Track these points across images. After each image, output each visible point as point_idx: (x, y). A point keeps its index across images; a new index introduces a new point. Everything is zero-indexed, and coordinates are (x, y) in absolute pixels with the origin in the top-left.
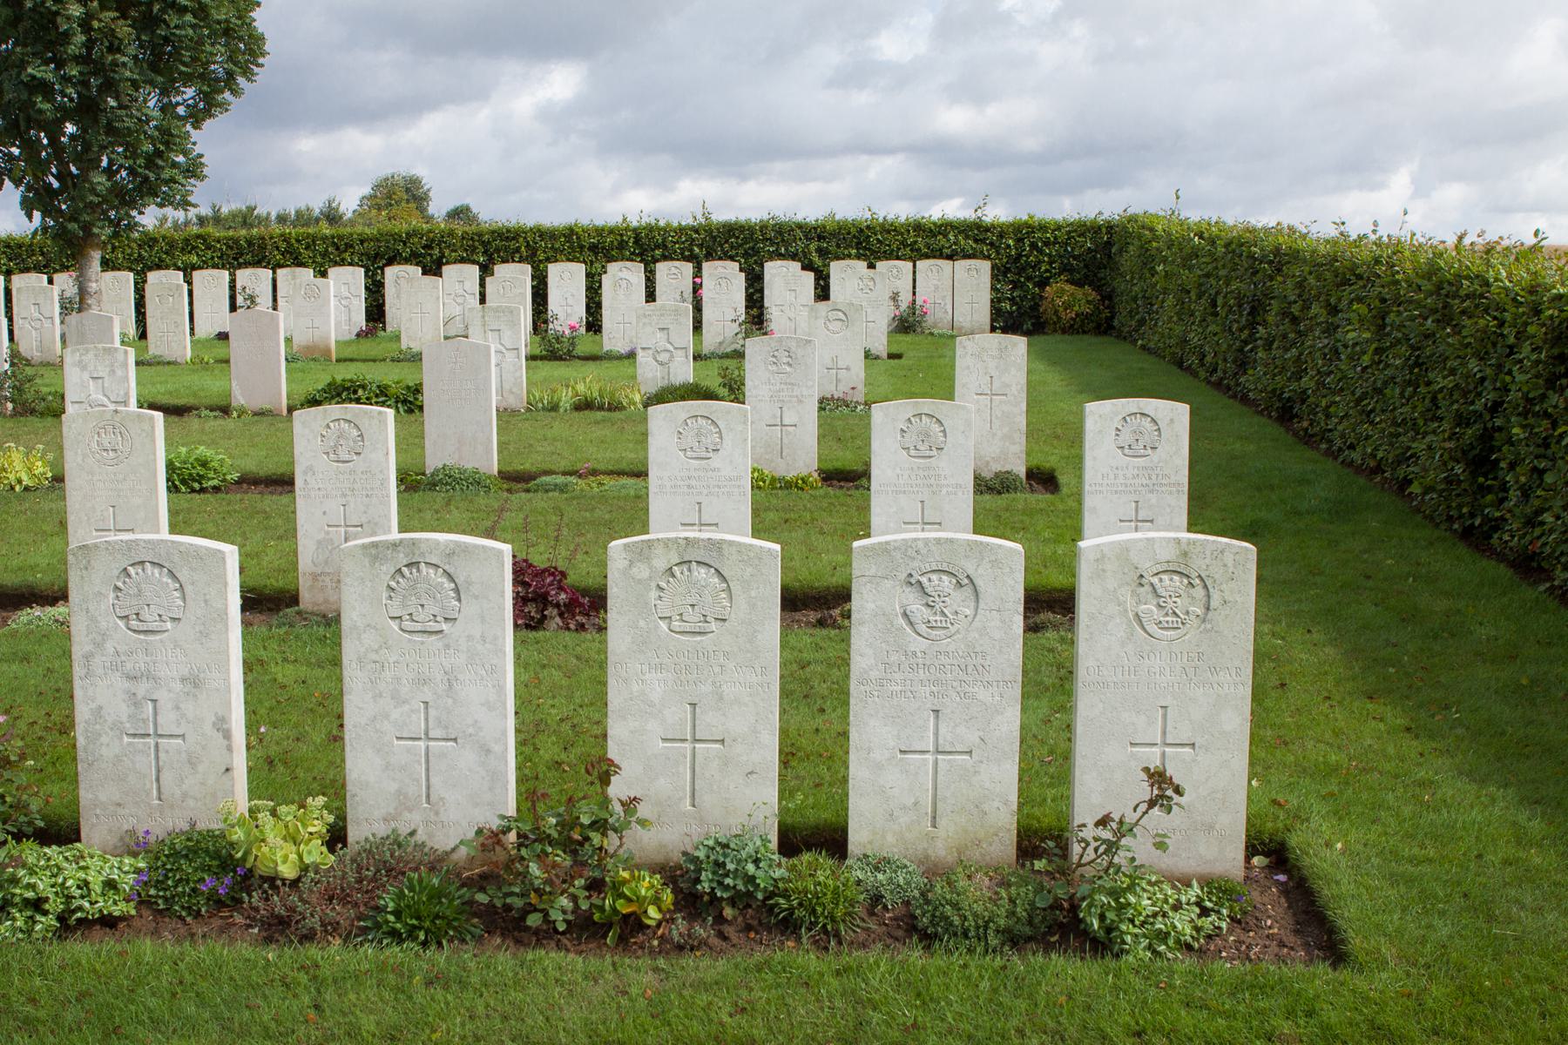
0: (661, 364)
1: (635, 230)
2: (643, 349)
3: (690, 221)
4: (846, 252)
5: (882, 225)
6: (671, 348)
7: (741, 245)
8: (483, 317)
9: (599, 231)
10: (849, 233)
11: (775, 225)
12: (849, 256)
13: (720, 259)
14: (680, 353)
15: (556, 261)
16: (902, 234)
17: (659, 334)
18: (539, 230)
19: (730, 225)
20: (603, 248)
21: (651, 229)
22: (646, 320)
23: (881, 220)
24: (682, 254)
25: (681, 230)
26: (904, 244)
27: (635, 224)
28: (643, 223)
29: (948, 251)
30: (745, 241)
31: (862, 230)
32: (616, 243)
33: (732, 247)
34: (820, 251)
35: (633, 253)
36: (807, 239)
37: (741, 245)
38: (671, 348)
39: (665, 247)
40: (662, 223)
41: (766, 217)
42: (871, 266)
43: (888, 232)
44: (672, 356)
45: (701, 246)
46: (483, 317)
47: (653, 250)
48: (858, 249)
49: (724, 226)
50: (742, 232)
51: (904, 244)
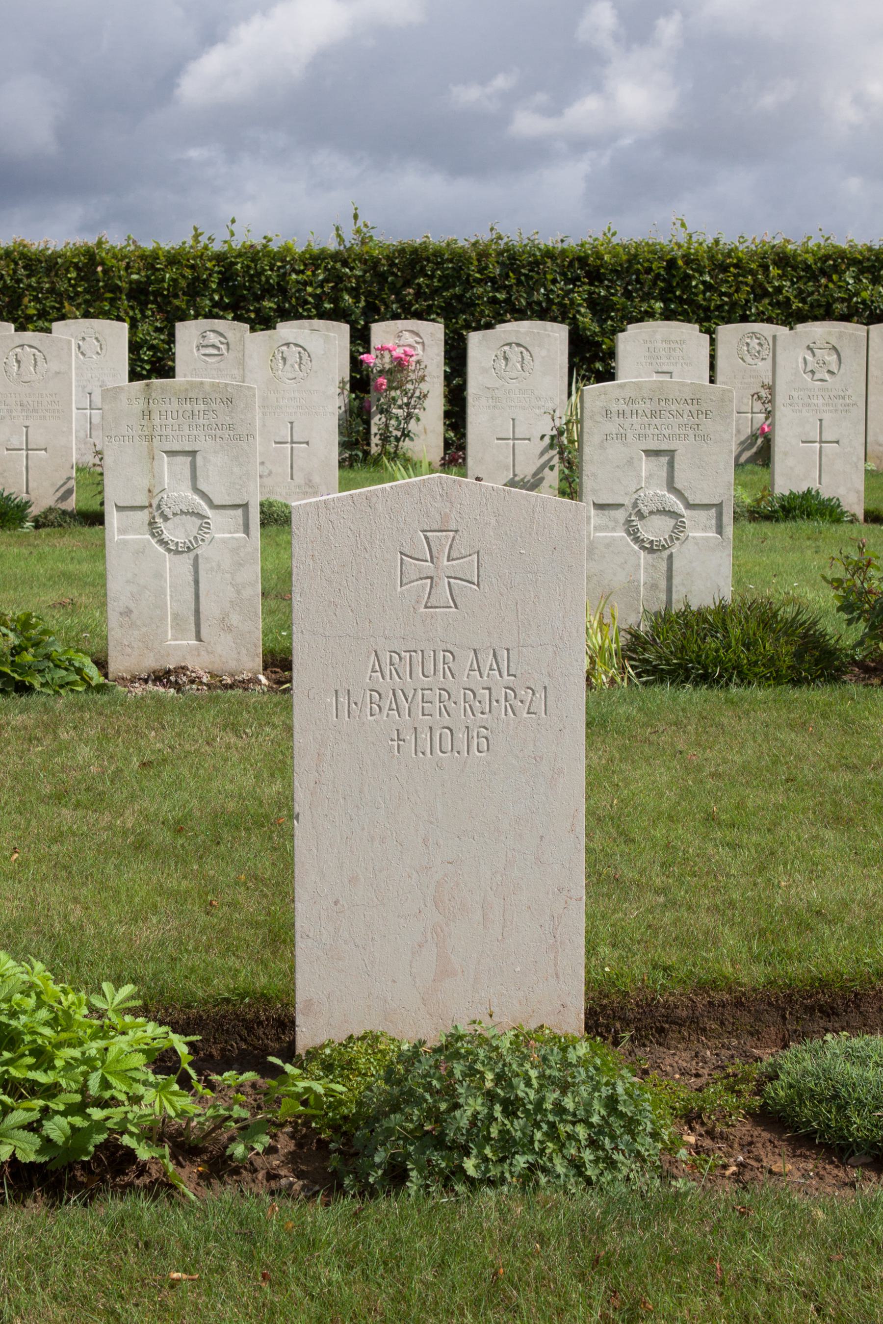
0: (651, 550)
1: (219, 258)
2: (119, 508)
3: (332, 245)
4: (644, 307)
5: (711, 254)
6: (680, 508)
7: (436, 291)
8: (147, 414)
9: (150, 260)
10: (649, 270)
11: (500, 253)
12: (649, 315)
13: (396, 317)
14: (701, 515)
15: (63, 317)
16: (752, 272)
17: (645, 465)
18: (23, 256)
19: (415, 251)
20: (158, 293)
21: (253, 255)
22: (611, 427)
23: (710, 241)
24: (318, 306)
25: (315, 260)
26: (760, 293)
27: (217, 247)
28: (237, 244)
29: (839, 307)
30: (447, 282)
31: (672, 263)
32: (183, 283)
33: (419, 294)
34: (593, 303)
35: (215, 305)
36: (568, 281)
37: (436, 291)
38: (680, 508)
39: (282, 290)
40: (274, 247)
41: (485, 237)
42: (791, 329)
43: (724, 268)
44: (680, 527)
45: (355, 293)
46: (147, 414)
47: (259, 299)
48: (664, 301)
49: (402, 251)
50: (439, 265)
51: (760, 293)
